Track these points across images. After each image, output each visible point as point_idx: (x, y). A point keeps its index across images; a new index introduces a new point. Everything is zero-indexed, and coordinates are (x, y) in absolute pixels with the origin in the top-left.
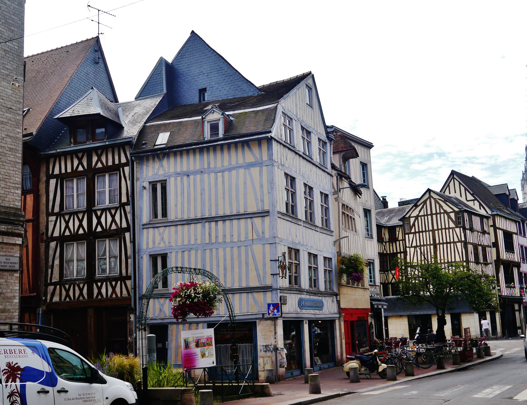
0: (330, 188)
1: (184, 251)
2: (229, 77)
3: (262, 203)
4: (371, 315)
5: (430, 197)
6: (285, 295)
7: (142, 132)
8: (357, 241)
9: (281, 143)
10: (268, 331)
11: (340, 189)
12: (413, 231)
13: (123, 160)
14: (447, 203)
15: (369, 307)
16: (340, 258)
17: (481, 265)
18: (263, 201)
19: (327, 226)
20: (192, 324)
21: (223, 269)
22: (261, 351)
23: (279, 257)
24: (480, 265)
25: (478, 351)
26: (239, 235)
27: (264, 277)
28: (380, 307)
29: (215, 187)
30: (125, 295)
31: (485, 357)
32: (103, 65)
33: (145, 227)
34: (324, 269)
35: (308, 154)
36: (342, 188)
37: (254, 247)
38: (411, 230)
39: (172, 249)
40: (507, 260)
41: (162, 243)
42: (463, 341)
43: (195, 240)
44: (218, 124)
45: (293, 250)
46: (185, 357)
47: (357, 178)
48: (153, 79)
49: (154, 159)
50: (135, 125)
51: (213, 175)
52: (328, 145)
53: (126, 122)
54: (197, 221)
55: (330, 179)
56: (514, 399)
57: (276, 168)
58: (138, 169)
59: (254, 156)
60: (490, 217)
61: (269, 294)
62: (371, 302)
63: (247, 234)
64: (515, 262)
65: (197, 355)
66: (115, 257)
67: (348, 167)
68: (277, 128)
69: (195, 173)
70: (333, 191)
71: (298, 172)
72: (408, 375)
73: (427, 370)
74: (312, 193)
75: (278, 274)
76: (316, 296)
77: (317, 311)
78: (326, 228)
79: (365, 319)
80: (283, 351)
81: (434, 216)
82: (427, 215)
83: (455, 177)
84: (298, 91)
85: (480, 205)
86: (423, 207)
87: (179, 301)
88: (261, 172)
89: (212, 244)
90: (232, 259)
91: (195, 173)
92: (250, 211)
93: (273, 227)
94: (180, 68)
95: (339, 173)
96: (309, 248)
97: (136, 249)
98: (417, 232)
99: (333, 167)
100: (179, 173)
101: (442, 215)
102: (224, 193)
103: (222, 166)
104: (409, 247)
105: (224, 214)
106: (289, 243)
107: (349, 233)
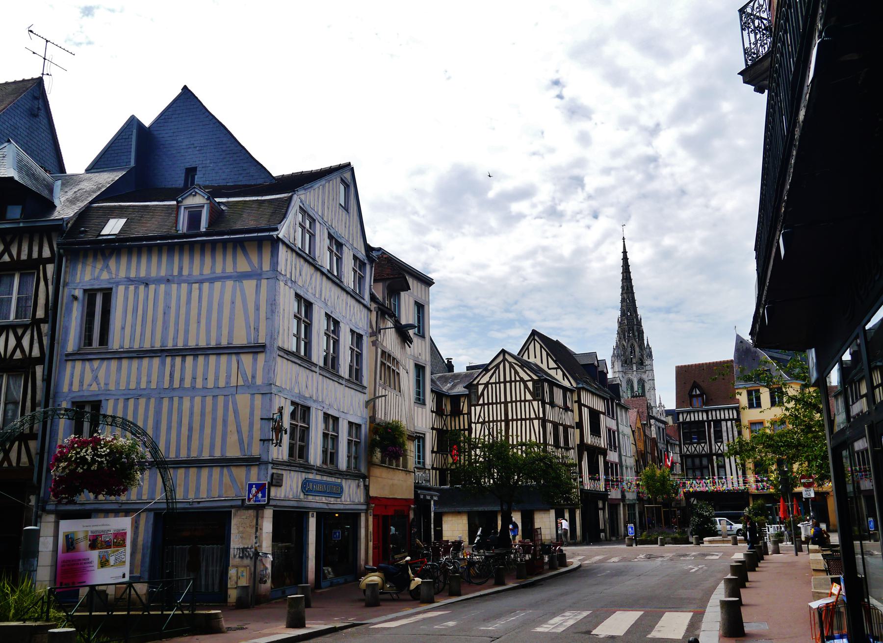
1: (128, 399)
2: (231, 155)
4: (414, 508)
5: (504, 360)
6: (280, 472)
7: (83, 216)
9: (292, 250)
12: (481, 402)
13: (47, 253)
14: (524, 368)
15: (413, 497)
16: (373, 425)
17: (561, 450)
18: (258, 331)
21: (188, 428)
22: (235, 556)
23: (273, 414)
26: (217, 379)
27: (250, 445)
28: (428, 498)
29: (187, 304)
30: (25, 463)
31: (558, 568)
32: (45, 121)
33: (70, 358)
34: (348, 440)
35: (336, 274)
37: (238, 397)
39: (109, 394)
41: (94, 384)
43: (147, 382)
44: (200, 213)
45: (300, 407)
46: (63, 566)
47: (407, 316)
48: (117, 145)
49: (95, 257)
50: (75, 204)
51: (184, 286)
52: (368, 267)
53: (62, 199)
54: (151, 353)
55: (367, 315)
56: (592, 633)
57: (282, 284)
58: (68, 269)
59: (250, 262)
61: (254, 471)
63: (229, 377)
64: (601, 448)
66: (16, 403)
68: (289, 227)
69: (158, 281)
70: (370, 331)
71: (317, 296)
72: (452, 594)
73: (481, 586)
75: (270, 440)
77: (332, 499)
80: (266, 557)
81: (508, 385)
82: (500, 383)
84: (327, 184)
85: (564, 374)
86: (495, 372)
87: (64, 468)
88: (258, 287)
89: (174, 389)
90: (203, 414)
91: (158, 281)
93: (269, 370)
95: (380, 307)
96: (326, 407)
97: (52, 392)
98: (486, 404)
99: (373, 298)
102: (199, 314)
104: (474, 423)
105: (196, 345)
106: (293, 396)
107: (391, 394)
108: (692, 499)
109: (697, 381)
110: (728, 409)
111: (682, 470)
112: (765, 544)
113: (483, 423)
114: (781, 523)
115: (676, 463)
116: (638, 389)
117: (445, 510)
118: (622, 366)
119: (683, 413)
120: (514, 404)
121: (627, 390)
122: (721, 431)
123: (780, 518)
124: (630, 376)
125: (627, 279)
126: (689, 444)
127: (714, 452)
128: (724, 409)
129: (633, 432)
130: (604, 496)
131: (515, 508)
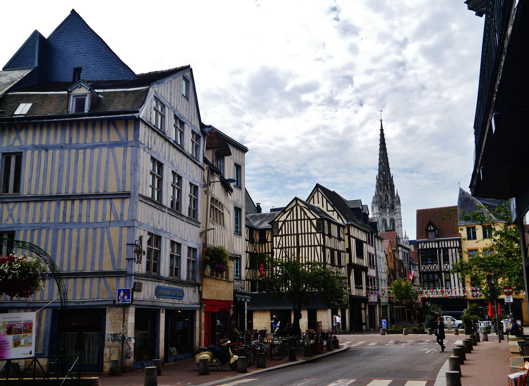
0: (200, 180)
3: (124, 184)
5: (297, 204)
6: (140, 281)
8: (224, 234)
9: (149, 127)
10: (118, 318)
11: (210, 183)
12: (280, 234)
15: (232, 299)
16: (205, 249)
17: (336, 267)
19: (194, 217)
20: (35, 309)
21: (75, 250)
22: (108, 340)
23: (136, 241)
24: (335, 267)
25: (328, 343)
26: (96, 216)
27: (119, 261)
28: (243, 300)
31: (333, 349)
34: (188, 259)
35: (179, 143)
36: (213, 181)
37: (111, 229)
38: (279, 232)
39: (21, 227)
40: (357, 265)
41: (10, 219)
42: (315, 334)
43: (47, 218)
45: (154, 237)
48: (25, 51)
49: (10, 130)
52: (202, 139)
54: (51, 198)
57: (142, 150)
59: (119, 135)
60: (346, 226)
61: (122, 280)
62: (234, 295)
64: (364, 267)
65: (8, 344)
67: (223, 167)
68: (147, 110)
69: (54, 148)
70: (203, 183)
71: (166, 159)
72: (259, 367)
74: (181, 182)
75: (133, 259)
76: (176, 285)
77: (176, 301)
78: (192, 218)
79: (227, 311)
80: (130, 340)
81: (299, 222)
82: (293, 220)
83: (319, 189)
85: (338, 215)
86: (290, 213)
88: (125, 152)
89: (66, 223)
90: (86, 241)
91: (54, 148)
92: (110, 190)
93: (133, 210)
94: (56, 45)
95: (211, 167)
96: (172, 236)
98: (284, 235)
99: (205, 160)
100: (37, 146)
101: (306, 221)
103: (84, 143)
104: (276, 248)
106: (149, 228)
108: (427, 303)
109: (431, 220)
110: (453, 240)
111: (420, 282)
112: (478, 334)
113: (282, 248)
114: (489, 320)
115: (416, 278)
116: (390, 226)
117: (255, 308)
118: (379, 209)
119: (421, 242)
120: (303, 235)
121: (382, 226)
122: (448, 256)
123: (489, 317)
124: (384, 217)
125: (383, 149)
126: (425, 264)
127: (443, 270)
128: (450, 240)
129: (386, 255)
130: (365, 300)
131: (304, 308)
